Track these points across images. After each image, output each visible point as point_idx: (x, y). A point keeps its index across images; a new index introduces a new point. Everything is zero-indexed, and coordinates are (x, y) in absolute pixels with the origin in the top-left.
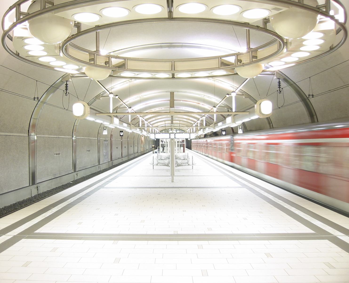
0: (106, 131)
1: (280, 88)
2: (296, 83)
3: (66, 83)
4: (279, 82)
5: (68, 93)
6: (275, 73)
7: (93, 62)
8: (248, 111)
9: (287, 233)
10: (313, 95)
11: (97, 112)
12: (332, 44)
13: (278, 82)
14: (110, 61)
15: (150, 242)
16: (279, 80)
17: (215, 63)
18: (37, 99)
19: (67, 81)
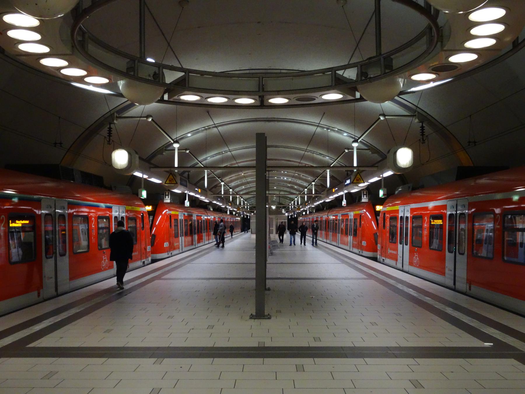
0: (168, 198)
1: (424, 136)
2: (447, 128)
3: (108, 126)
4: (422, 127)
5: (113, 141)
6: (417, 115)
7: (132, 73)
8: (376, 165)
9: (444, 346)
10: (475, 142)
11: (152, 166)
12: (517, 36)
13: (420, 127)
14: (161, 72)
15: (269, 361)
16: (422, 124)
17: (327, 80)
18: (60, 145)
19: (110, 124)
